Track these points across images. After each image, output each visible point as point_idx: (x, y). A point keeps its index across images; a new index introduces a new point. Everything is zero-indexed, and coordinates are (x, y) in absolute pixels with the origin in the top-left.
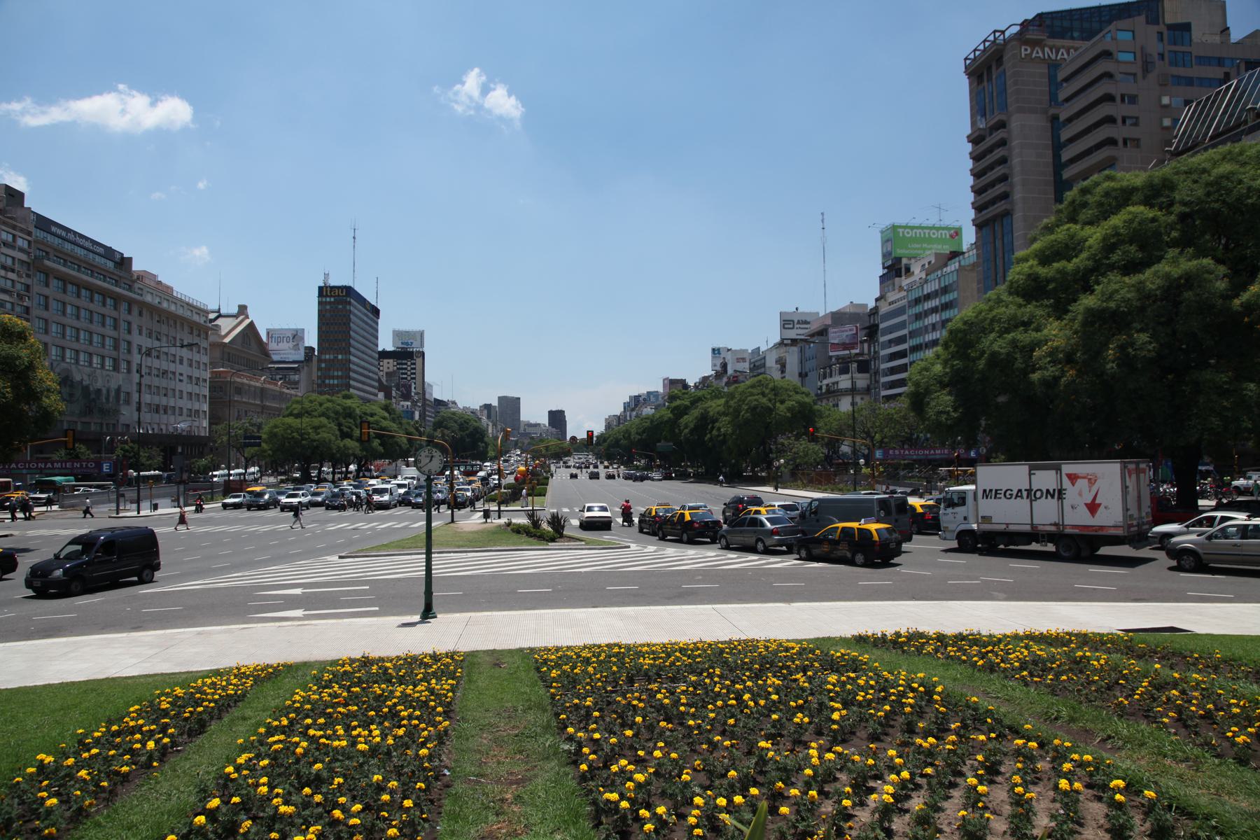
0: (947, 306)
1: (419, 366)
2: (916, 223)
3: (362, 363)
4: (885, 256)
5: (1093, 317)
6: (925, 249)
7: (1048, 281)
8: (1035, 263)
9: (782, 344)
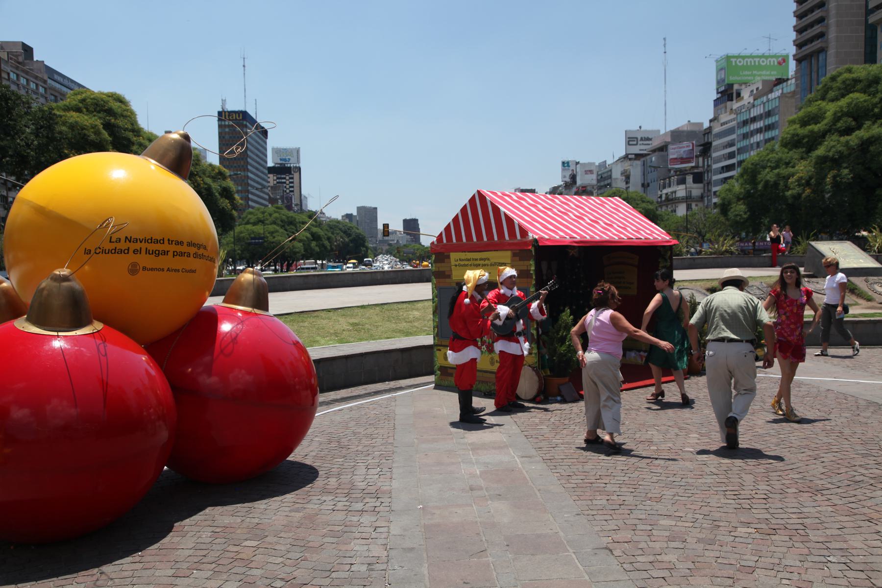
0: (769, 128)
1: (296, 180)
2: (747, 53)
3: (256, 178)
4: (719, 82)
5: (822, 161)
6: (755, 75)
7: (804, 137)
8: (798, 126)
9: (626, 157)
